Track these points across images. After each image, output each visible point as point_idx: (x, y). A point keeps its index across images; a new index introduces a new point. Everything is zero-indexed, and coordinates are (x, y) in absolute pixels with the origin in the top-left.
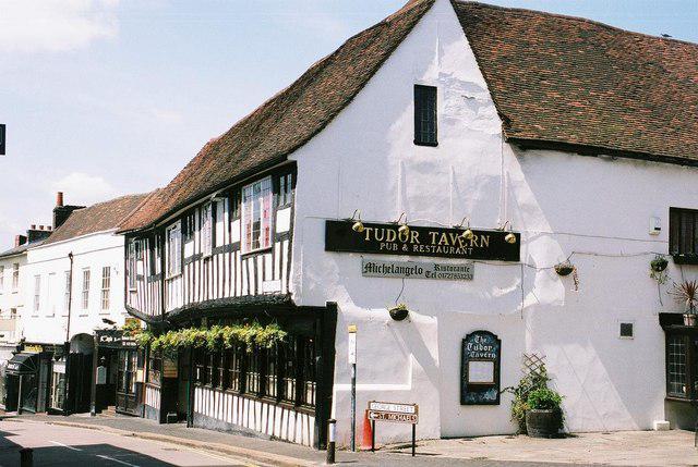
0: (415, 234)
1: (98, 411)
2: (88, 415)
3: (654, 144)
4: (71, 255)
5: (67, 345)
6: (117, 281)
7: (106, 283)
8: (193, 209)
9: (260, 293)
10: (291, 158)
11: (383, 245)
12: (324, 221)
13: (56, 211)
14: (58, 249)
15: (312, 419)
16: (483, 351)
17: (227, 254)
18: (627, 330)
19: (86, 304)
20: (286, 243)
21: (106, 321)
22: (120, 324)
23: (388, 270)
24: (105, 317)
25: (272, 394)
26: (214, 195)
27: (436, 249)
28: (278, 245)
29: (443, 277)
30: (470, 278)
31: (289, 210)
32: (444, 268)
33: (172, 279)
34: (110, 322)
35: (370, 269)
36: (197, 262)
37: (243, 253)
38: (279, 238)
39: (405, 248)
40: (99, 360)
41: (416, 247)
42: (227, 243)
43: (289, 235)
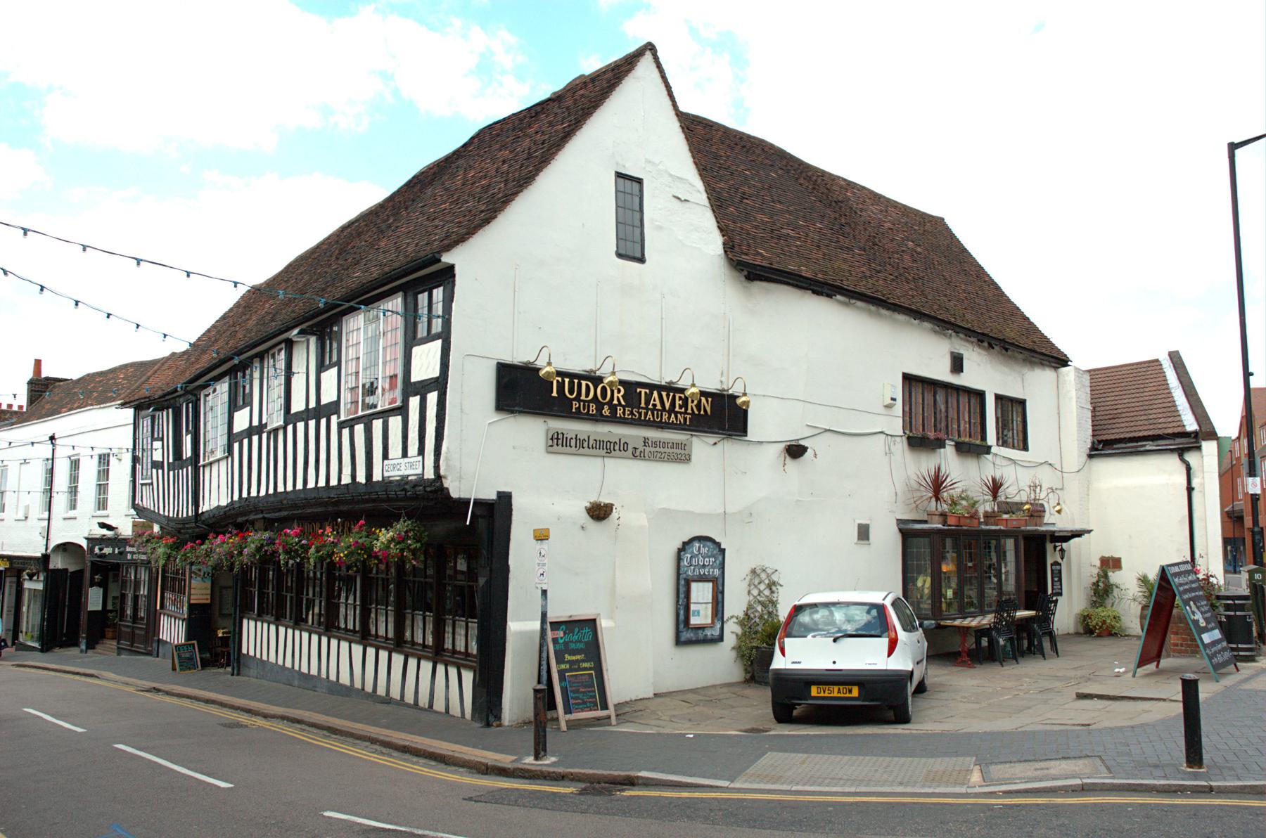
0: (619, 391)
1: (91, 646)
2: (74, 651)
3: (897, 296)
4: (52, 438)
5: (46, 558)
6: (120, 472)
7: (104, 473)
8: (252, 358)
9: (377, 477)
10: (447, 258)
11: (575, 405)
12: (495, 362)
13: (30, 383)
14: (40, 430)
15: (468, 677)
16: (704, 566)
17: (312, 423)
18: (864, 533)
19: (73, 506)
20: (432, 397)
21: (103, 525)
22: (126, 530)
23: (580, 445)
24: (101, 520)
25: (382, 632)
26: (296, 331)
27: (646, 414)
28: (414, 402)
29: (654, 458)
30: (686, 459)
31: (438, 344)
32: (656, 443)
33: (211, 464)
34: (109, 528)
35: (557, 442)
36: (255, 438)
37: (343, 418)
38: (422, 389)
39: (606, 411)
40: (92, 579)
41: (620, 412)
42: (312, 404)
43: (440, 384)
